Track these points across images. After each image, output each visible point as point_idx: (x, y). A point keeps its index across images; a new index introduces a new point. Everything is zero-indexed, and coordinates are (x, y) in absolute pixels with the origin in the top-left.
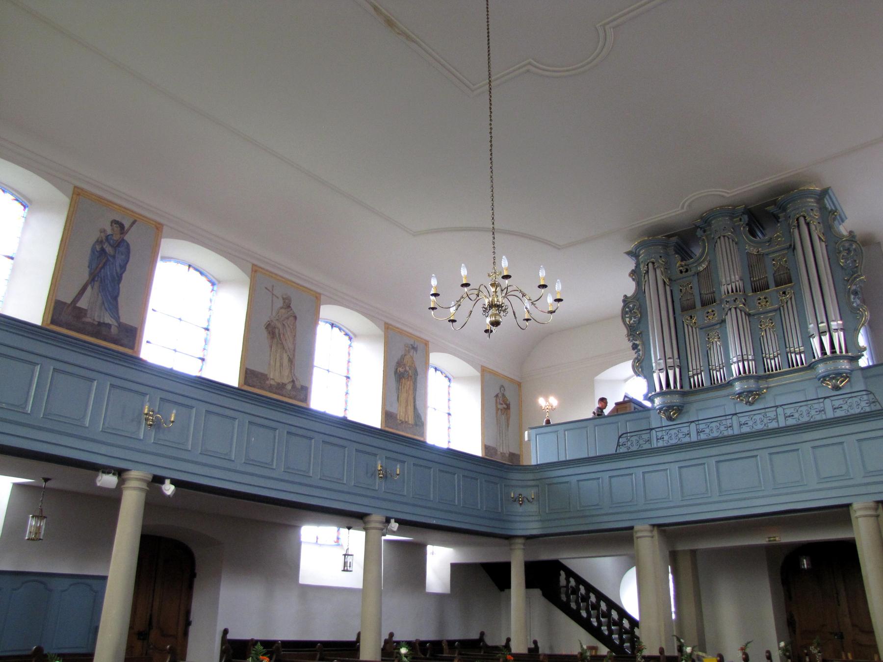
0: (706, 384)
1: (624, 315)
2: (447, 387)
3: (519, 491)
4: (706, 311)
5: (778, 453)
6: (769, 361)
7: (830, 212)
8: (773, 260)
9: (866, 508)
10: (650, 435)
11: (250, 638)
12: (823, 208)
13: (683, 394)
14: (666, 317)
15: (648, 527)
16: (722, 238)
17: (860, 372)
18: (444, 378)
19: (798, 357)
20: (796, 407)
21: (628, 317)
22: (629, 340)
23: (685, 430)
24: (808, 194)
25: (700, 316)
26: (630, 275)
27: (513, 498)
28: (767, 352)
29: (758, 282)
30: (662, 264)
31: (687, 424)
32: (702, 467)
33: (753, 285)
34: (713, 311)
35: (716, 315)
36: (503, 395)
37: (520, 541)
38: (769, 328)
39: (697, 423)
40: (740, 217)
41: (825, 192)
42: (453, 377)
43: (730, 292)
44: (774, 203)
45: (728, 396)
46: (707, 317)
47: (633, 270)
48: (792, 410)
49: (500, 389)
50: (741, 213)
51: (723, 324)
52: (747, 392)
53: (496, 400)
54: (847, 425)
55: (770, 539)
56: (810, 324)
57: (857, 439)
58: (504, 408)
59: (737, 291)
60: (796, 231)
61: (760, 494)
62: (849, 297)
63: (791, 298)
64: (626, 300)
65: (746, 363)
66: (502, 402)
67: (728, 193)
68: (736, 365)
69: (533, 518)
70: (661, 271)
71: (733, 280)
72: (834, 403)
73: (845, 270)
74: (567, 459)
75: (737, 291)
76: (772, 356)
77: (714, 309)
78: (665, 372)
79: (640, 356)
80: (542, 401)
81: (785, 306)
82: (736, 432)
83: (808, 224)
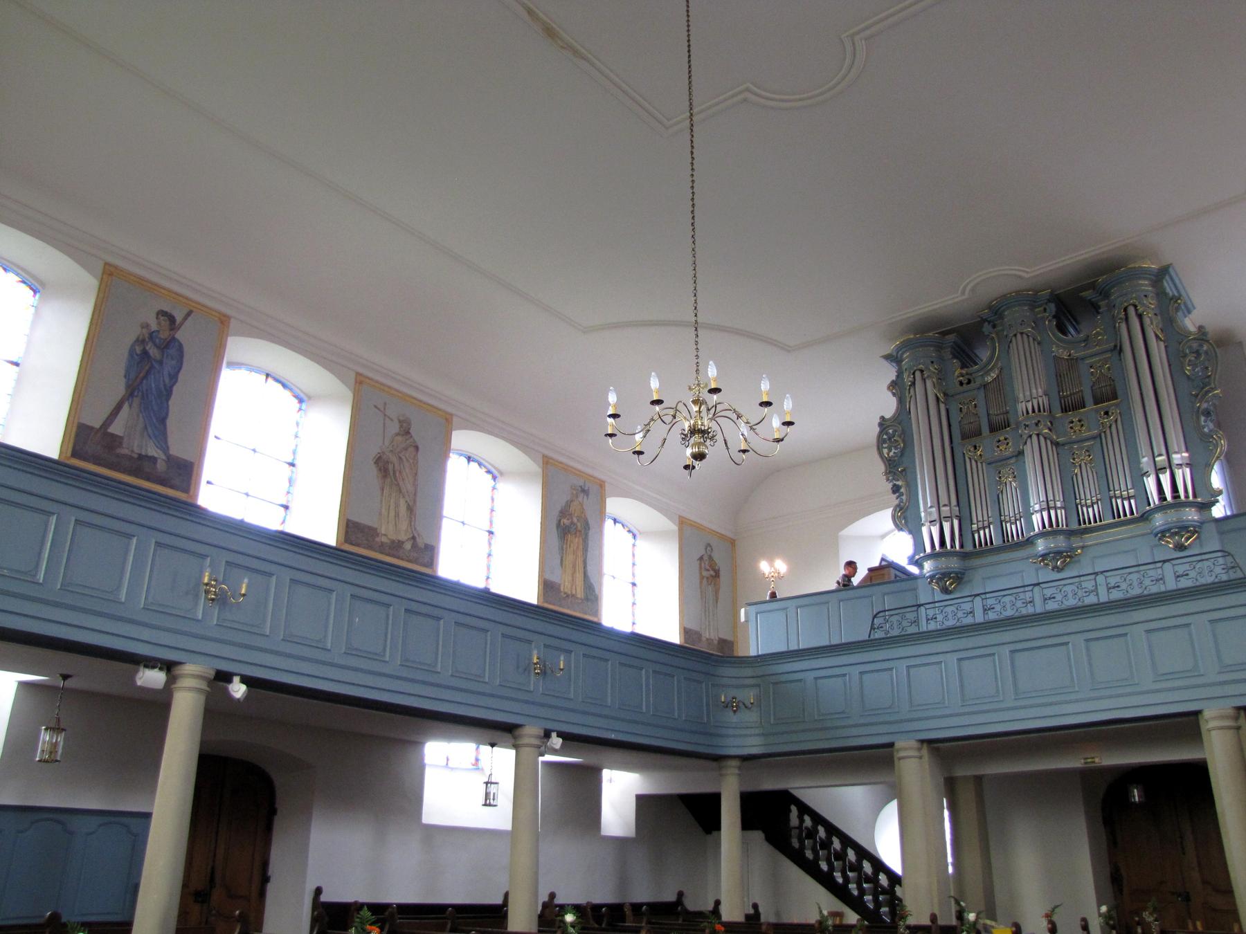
0: (997, 541)
1: (880, 445)
2: (631, 546)
3: (733, 692)
4: (996, 439)
5: (1098, 639)
6: (1085, 509)
7: (1171, 299)
8: (1091, 367)
9: (1222, 717)
10: (918, 614)
11: (353, 901)
12: (1161, 294)
13: (964, 556)
14: (940, 447)
15: (914, 744)
16: (1019, 336)
17: (1213, 525)
18: (627, 533)
19: (1126, 503)
20: (1124, 574)
21: (886, 448)
22: (888, 480)
23: (967, 607)
24: (1140, 273)
25: (987, 446)
26: (888, 388)
27: (723, 702)
28: (1083, 497)
29: (1069, 398)
30: (934, 373)
31: (969, 599)
32: (991, 658)
33: (1063, 402)
34: (1006, 439)
35: (1010, 444)
36: (710, 558)
37: (734, 763)
38: (1085, 463)
39: (983, 596)
40: (1045, 306)
41: (1164, 271)
42: (639, 531)
43: (1030, 411)
44: (1092, 286)
45: (1027, 558)
46: (998, 447)
47: (893, 382)
48: (1118, 579)
49: (706, 549)
50: (1046, 301)
51: (1020, 457)
52: (1054, 553)
53: (700, 565)
54: (1195, 599)
55: (1086, 761)
56: (1143, 457)
57: (1209, 619)
58: (712, 576)
59: (1039, 411)
60: (1124, 326)
61: (1073, 697)
62: (1198, 418)
63: (1116, 421)
64: (883, 423)
65: (1052, 513)
66: (708, 568)
67: (1027, 272)
68: (1038, 515)
69: (753, 731)
70: (933, 382)
71: (1035, 395)
72: (1177, 568)
73: (1193, 380)
74: (801, 647)
75: (1039, 411)
76: (1089, 502)
77: (1007, 436)
78: (938, 525)
79: (902, 502)
80: (764, 566)
81: (1108, 432)
82: (1039, 610)
83: (1140, 316)
